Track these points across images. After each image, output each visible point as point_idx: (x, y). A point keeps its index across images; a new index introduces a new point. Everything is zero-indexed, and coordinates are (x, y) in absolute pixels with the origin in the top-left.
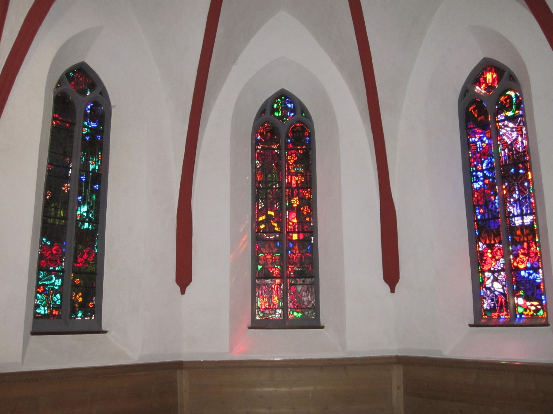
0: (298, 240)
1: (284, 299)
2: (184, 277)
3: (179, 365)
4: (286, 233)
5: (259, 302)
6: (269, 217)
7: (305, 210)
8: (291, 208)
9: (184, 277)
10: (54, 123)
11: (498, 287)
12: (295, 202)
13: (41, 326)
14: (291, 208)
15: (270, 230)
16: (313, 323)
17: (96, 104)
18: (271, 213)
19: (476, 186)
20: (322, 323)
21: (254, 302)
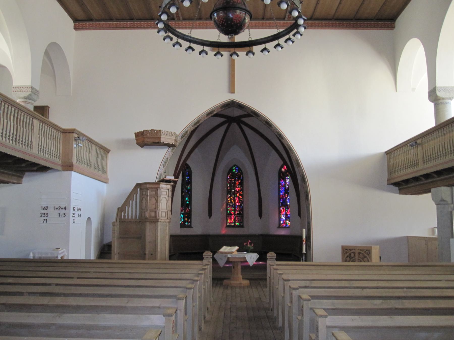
0: (238, 205)
1: (234, 220)
2: (210, 214)
3: (209, 236)
4: (235, 204)
5: (228, 221)
6: (231, 199)
7: (240, 197)
8: (237, 197)
9: (210, 214)
10: (189, 188)
11: (284, 218)
12: (238, 195)
13: (183, 225)
14: (237, 197)
15: (231, 202)
16: (190, 226)
17: (189, 172)
18: (232, 198)
19: (281, 194)
20: (192, 226)
21: (227, 220)
